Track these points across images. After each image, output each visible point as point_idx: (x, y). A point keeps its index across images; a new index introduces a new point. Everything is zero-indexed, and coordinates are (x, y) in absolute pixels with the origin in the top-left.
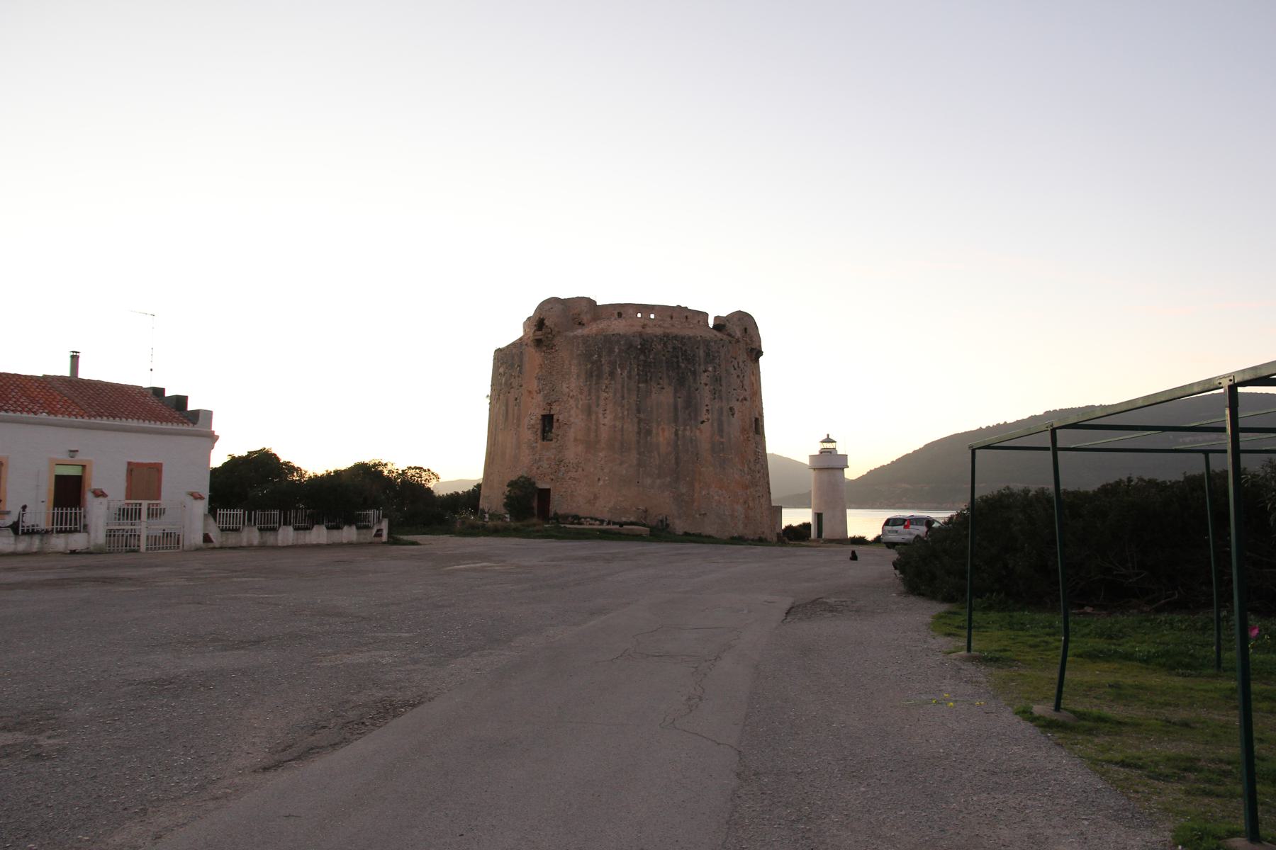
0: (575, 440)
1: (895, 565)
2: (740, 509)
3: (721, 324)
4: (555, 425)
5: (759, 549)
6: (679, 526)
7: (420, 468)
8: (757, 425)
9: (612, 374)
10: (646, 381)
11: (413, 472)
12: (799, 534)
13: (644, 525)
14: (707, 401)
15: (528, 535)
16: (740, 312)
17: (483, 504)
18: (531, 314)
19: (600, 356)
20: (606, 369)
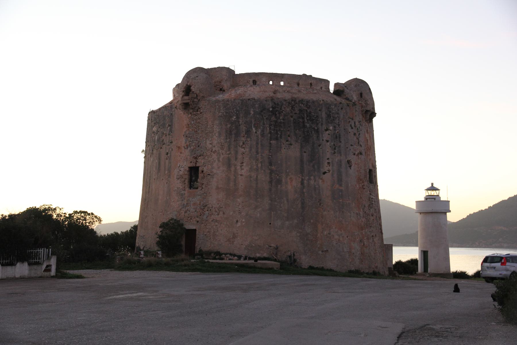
0: (218, 188)
1: (494, 297)
2: (356, 246)
3: (340, 90)
4: (200, 175)
5: (373, 282)
6: (305, 261)
7: (85, 212)
8: (370, 176)
9: (248, 132)
10: (277, 139)
11: (78, 215)
12: (407, 268)
13: (275, 260)
14: (328, 155)
15: (177, 269)
16: (356, 79)
17: (139, 242)
18: (179, 81)
19: (238, 117)
20: (243, 128)
